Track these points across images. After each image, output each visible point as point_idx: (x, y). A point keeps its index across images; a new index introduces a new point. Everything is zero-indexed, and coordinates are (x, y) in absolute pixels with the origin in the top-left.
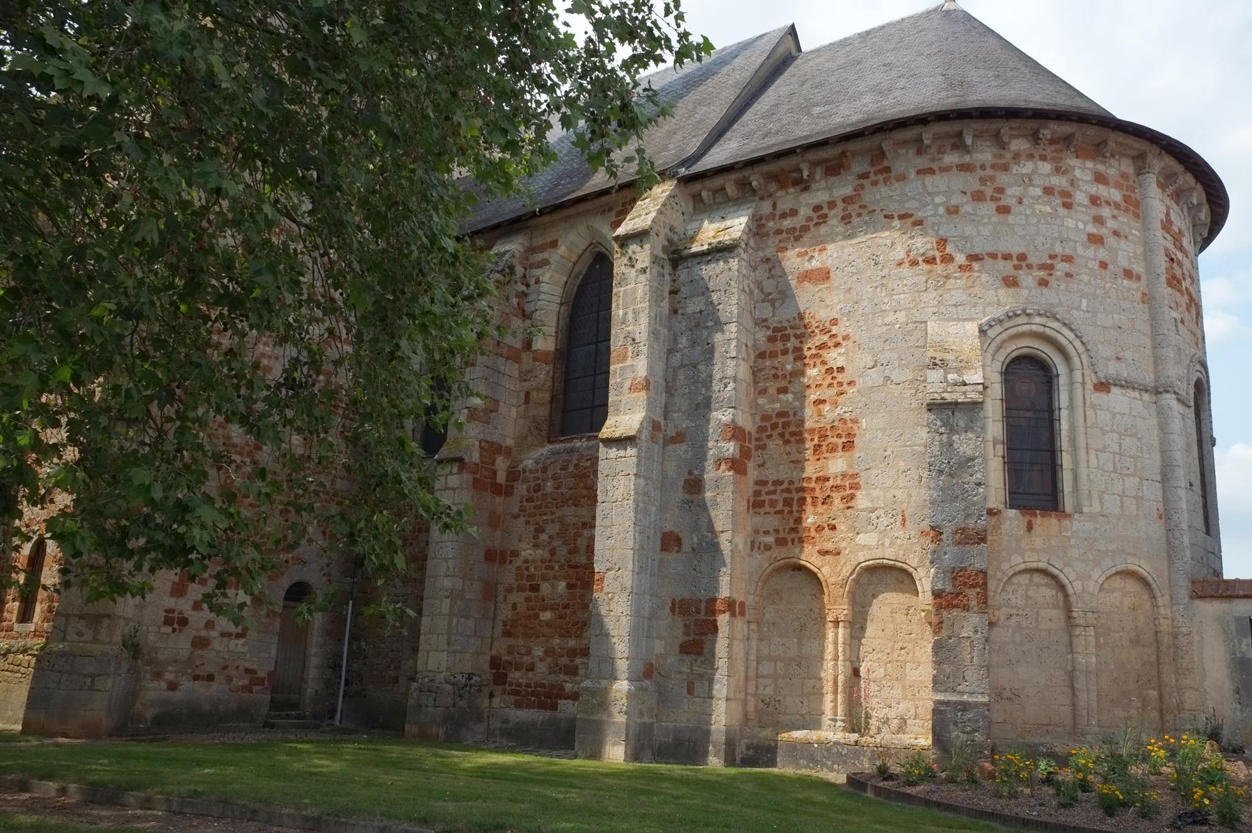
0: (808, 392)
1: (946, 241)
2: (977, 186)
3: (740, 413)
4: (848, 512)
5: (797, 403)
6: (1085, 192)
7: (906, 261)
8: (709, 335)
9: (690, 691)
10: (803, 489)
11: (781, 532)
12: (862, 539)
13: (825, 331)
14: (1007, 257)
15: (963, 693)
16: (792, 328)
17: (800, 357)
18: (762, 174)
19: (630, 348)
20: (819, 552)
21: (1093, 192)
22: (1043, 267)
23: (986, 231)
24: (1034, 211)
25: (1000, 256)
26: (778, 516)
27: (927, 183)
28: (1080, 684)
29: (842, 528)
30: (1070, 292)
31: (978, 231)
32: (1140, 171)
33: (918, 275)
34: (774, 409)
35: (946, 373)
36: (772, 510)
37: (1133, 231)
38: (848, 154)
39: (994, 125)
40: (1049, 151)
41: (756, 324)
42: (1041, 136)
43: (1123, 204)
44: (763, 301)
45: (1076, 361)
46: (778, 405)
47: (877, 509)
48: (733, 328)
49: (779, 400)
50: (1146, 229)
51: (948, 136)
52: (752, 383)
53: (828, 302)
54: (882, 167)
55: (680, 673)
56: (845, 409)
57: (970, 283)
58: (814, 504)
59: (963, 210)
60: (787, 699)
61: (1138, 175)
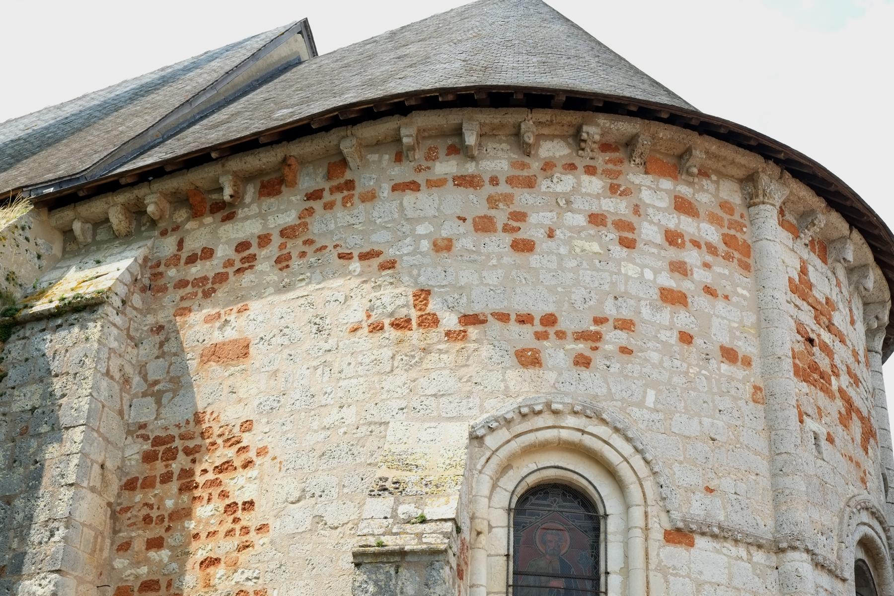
0: (194, 545)
1: (428, 292)
2: (482, 209)
3: (70, 581)
5: (174, 565)
6: (659, 224)
7: (365, 325)
8: (40, 449)
13: (232, 441)
14: (524, 319)
16: (182, 437)
17: (188, 486)
18: (164, 195)
21: (672, 225)
22: (582, 336)
23: (492, 278)
24: (572, 248)
25: (513, 317)
27: (405, 203)
30: (626, 377)
31: (481, 278)
32: (751, 202)
33: (380, 347)
34: (137, 577)
35: (398, 503)
37: (739, 290)
38: (292, 161)
39: (510, 117)
40: (601, 160)
41: (129, 433)
42: (585, 136)
43: (722, 248)
44: (144, 395)
46: (144, 570)
48: (77, 434)
49: (147, 561)
50: (760, 287)
51: (442, 134)
52: (107, 532)
53: (242, 393)
54: (342, 181)
56: (248, 574)
57: (461, 360)
59: (458, 246)
61: (749, 206)
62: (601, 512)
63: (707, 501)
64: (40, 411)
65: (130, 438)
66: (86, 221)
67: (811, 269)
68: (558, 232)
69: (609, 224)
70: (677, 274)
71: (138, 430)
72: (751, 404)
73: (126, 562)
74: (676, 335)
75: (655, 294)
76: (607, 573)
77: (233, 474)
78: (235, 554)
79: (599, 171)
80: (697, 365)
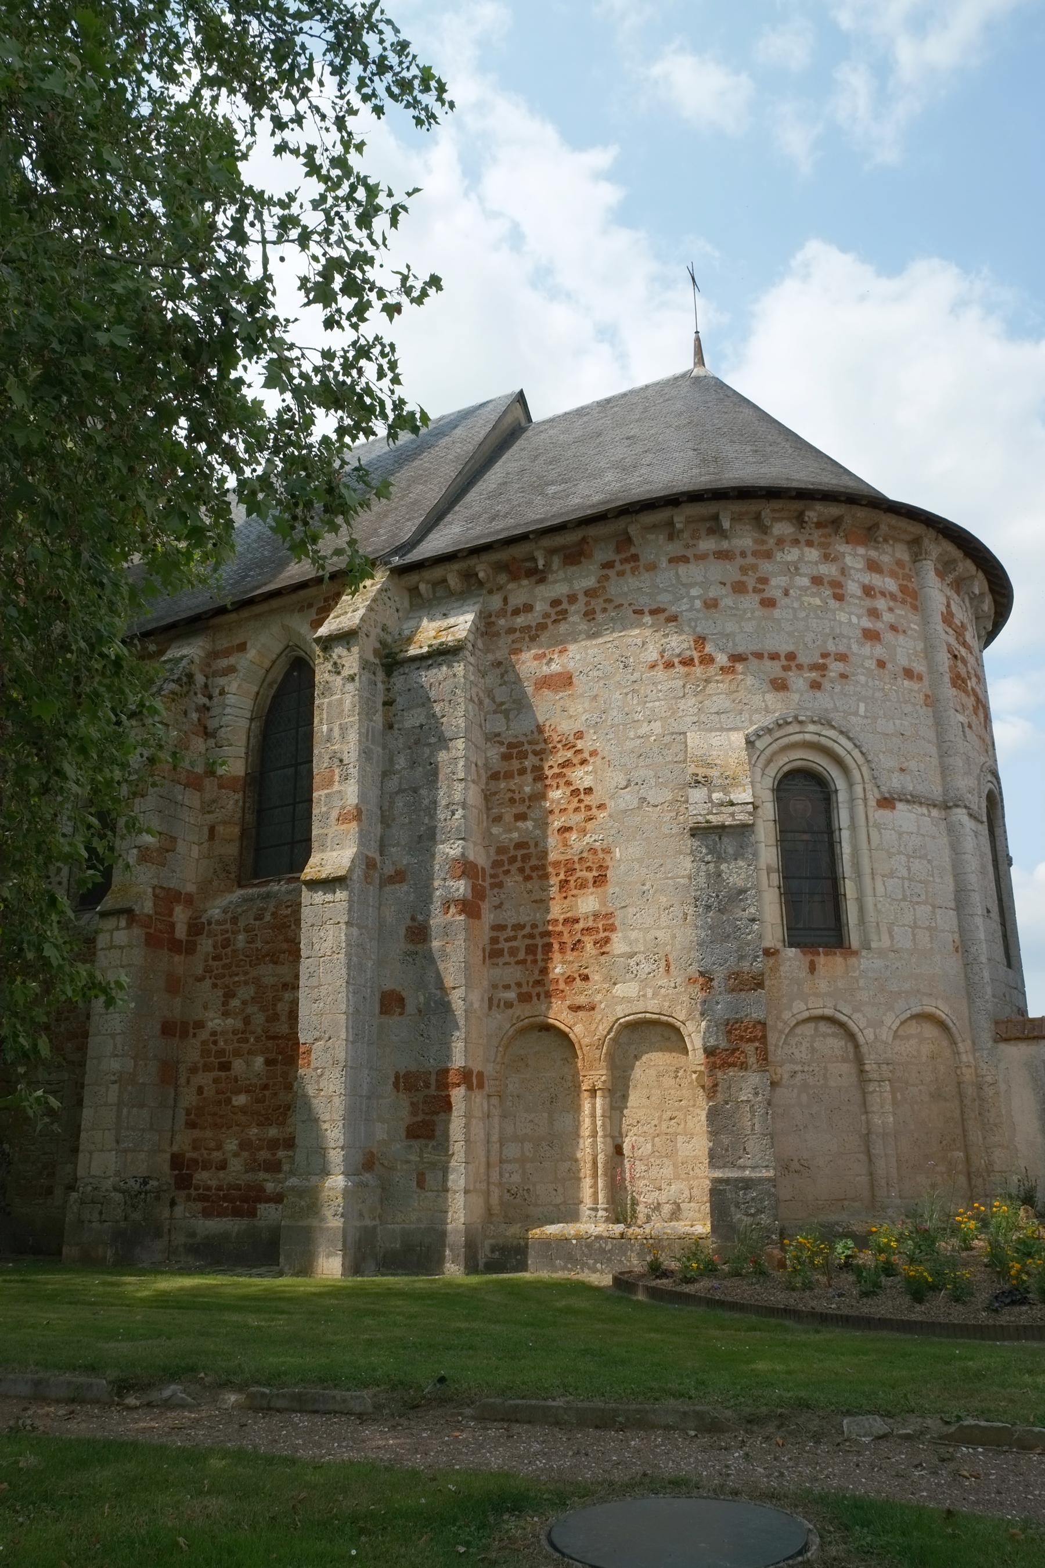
0: (551, 818)
1: (704, 639)
2: (737, 576)
3: (471, 845)
4: (603, 959)
5: (538, 832)
6: (858, 581)
7: (660, 663)
8: (432, 754)
9: (421, 1184)
10: (548, 934)
11: (525, 986)
12: (619, 990)
14: (774, 657)
15: (743, 1168)
16: (529, 743)
17: (539, 776)
19: (337, 771)
20: (570, 1008)
22: (815, 667)
23: (749, 627)
24: (802, 603)
25: (766, 655)
26: (520, 967)
28: (877, 1149)
29: (596, 978)
30: (845, 695)
31: (741, 627)
34: (511, 840)
35: (710, 792)
36: (512, 960)
37: (912, 625)
38: (590, 540)
40: (816, 535)
41: (488, 739)
42: (806, 519)
43: (899, 595)
44: (495, 712)
45: (856, 773)
46: (515, 835)
47: (636, 953)
48: (460, 744)
49: (517, 829)
50: (925, 622)
51: (703, 519)
52: (484, 810)
54: (629, 555)
55: (408, 1162)
57: (733, 687)
58: (562, 950)
59: (722, 604)
60: (538, 1187)
61: (915, 562)
62: (833, 788)
63: (902, 778)
64: (427, 727)
65: (489, 744)
66: (428, 583)
67: (952, 602)
68: (791, 591)
69: (825, 583)
70: (872, 618)
71: (493, 738)
72: (924, 708)
73: (501, 830)
74: (875, 662)
75: (859, 633)
76: (840, 829)
77: (573, 769)
78: (583, 824)
79: (816, 543)
80: (890, 683)
